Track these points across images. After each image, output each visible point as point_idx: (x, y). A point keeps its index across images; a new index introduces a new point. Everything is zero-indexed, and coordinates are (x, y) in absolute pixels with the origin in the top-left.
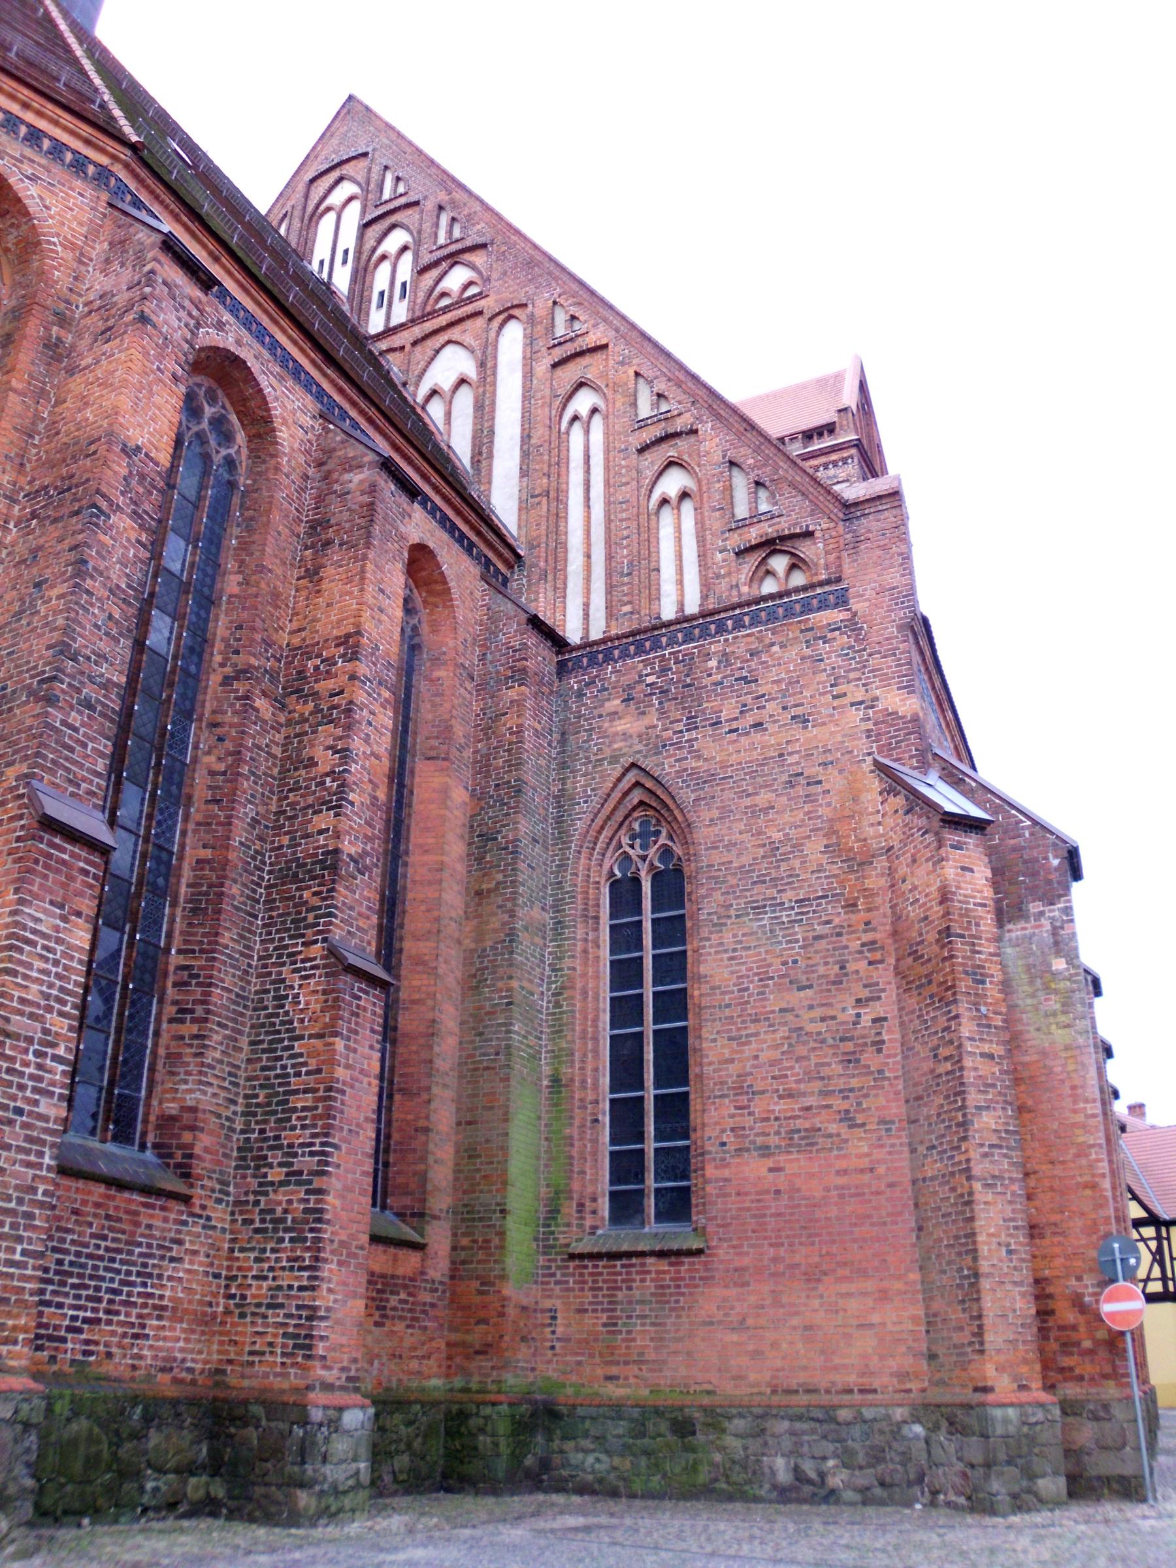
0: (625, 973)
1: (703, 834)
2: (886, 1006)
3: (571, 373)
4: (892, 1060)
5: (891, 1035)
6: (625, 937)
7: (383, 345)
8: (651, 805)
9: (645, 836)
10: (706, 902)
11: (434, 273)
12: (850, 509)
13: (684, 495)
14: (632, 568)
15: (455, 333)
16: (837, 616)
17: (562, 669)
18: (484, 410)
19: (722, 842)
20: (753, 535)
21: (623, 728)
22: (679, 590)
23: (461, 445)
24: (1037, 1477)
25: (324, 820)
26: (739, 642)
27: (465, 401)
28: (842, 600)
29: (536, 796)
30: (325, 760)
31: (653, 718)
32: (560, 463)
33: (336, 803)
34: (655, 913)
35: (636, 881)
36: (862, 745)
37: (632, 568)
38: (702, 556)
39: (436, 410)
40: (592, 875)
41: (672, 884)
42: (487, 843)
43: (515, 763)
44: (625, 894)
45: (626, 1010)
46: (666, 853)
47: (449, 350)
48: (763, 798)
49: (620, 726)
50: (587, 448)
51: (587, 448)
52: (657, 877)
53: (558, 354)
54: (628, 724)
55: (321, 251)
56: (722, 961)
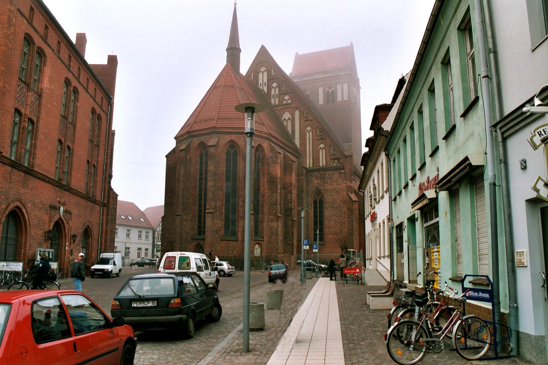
0: (315, 212)
1: (325, 197)
2: (346, 219)
3: (307, 123)
4: (346, 226)
5: (346, 223)
6: (315, 208)
7: (275, 109)
8: (318, 192)
9: (318, 196)
10: (326, 206)
11: (283, 95)
12: (346, 157)
13: (323, 148)
14: (316, 159)
15: (288, 109)
16: (343, 171)
17: (307, 172)
18: (293, 126)
19: (328, 198)
20: (333, 157)
21: (316, 182)
22: (322, 162)
23: (290, 129)
24: (59, 306)
25: (290, 205)
26: (331, 172)
27: (290, 123)
28: (344, 169)
29: (305, 191)
30: (290, 198)
31: (319, 181)
32: (305, 139)
33: (291, 203)
34: (319, 206)
35: (317, 201)
36: (345, 189)
37: (316, 159)
38: (326, 158)
39: (285, 122)
40: (311, 200)
41: (321, 202)
42: (299, 196)
43: (302, 187)
44: (315, 202)
45: (315, 217)
46: (320, 198)
47: (287, 112)
48: (333, 194)
49: (315, 181)
50: (309, 136)
51: (309, 136)
52: (319, 201)
53: (305, 119)
54: (316, 181)
55: (260, 81)
56: (328, 213)
